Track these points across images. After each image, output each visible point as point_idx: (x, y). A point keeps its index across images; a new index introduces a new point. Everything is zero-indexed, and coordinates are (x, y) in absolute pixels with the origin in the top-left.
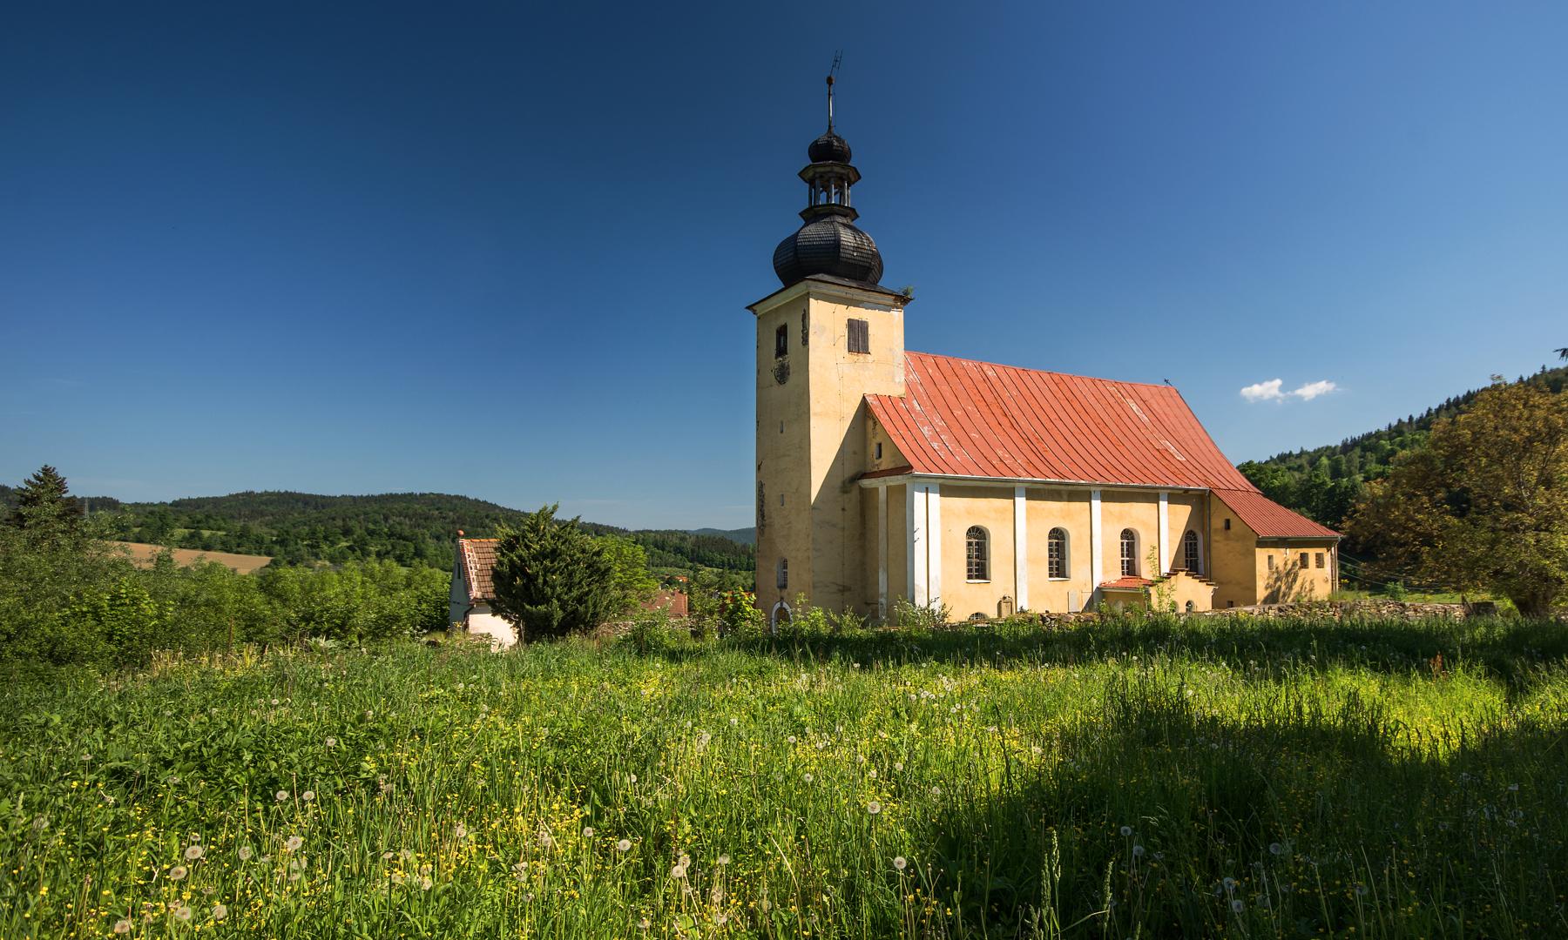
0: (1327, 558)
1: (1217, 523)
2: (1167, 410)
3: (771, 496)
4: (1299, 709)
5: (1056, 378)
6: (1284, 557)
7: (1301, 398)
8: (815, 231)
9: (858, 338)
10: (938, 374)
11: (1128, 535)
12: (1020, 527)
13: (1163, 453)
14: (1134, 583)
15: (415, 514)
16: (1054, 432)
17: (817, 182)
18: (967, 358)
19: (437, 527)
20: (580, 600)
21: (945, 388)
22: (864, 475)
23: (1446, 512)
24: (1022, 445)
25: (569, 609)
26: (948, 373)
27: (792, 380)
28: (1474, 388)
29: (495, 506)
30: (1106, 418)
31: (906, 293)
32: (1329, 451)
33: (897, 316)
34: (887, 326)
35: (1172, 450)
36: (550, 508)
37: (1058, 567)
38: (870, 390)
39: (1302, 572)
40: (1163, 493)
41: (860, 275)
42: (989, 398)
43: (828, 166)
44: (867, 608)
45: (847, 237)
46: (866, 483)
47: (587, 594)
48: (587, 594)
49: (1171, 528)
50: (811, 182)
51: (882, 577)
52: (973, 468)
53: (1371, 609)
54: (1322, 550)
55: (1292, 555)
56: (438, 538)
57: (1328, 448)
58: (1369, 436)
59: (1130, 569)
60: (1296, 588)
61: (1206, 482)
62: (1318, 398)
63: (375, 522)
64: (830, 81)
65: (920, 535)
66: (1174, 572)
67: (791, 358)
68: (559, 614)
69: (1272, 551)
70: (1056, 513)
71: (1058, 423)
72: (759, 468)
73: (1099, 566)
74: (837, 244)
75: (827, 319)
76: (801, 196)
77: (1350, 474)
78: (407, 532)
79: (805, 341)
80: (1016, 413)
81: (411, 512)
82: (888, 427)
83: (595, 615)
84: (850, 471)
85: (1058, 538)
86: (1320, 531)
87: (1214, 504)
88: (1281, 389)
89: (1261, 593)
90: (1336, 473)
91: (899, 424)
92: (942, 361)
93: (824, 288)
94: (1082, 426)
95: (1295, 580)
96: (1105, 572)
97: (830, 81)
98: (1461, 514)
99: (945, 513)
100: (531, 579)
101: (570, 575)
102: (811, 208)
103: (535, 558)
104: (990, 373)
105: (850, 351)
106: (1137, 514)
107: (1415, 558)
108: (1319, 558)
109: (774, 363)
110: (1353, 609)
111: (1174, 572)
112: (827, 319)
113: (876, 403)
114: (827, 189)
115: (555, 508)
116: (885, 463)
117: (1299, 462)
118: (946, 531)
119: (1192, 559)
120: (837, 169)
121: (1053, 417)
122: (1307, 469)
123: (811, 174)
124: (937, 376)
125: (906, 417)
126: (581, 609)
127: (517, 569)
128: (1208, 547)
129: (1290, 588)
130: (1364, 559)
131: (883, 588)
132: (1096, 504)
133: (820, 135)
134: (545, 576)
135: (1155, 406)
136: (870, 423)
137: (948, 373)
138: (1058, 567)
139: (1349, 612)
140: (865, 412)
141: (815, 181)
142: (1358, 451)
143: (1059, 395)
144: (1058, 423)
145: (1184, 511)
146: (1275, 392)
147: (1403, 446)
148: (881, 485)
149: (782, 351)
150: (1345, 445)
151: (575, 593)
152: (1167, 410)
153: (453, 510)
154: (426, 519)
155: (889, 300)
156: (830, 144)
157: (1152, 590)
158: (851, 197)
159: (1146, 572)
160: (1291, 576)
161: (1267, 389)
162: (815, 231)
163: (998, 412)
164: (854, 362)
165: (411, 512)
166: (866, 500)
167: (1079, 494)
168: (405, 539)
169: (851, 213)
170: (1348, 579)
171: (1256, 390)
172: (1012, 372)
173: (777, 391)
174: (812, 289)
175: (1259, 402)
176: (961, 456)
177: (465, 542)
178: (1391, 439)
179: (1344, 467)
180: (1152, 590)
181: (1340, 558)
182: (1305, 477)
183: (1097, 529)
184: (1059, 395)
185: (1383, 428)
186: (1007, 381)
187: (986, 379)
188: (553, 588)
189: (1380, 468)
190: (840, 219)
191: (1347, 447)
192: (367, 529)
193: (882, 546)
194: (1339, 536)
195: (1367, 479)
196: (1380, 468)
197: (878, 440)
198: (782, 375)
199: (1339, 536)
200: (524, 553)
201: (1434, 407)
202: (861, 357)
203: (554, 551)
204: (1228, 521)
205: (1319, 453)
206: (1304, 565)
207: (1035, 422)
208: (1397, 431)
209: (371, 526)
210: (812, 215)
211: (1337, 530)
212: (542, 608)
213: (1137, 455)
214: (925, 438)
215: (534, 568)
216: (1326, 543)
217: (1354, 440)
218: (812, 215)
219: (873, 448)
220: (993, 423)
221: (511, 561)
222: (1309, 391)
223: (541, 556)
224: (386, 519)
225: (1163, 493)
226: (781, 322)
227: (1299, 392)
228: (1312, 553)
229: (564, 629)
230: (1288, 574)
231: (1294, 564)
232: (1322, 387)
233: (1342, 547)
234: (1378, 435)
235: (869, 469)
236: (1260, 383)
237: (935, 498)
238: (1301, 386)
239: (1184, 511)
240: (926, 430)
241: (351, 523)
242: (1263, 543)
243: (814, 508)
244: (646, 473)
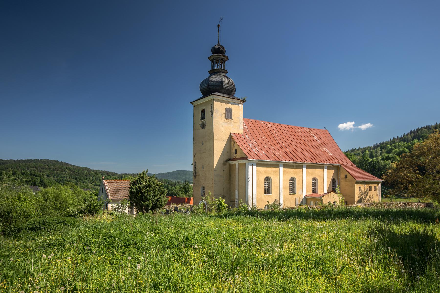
0: (378, 187)
1: (342, 176)
2: (325, 138)
3: (199, 165)
4: (401, 232)
5: (290, 127)
6: (364, 187)
7: (360, 129)
8: (214, 78)
9: (229, 114)
10: (253, 126)
11: (314, 179)
12: (281, 177)
13: (324, 152)
14: (315, 195)
15: (39, 167)
16: (290, 145)
17: (215, 61)
18: (262, 120)
19: (48, 172)
20: (157, 200)
21: (255, 131)
22: (230, 160)
23: (418, 173)
24: (281, 150)
25: (154, 203)
26: (256, 125)
27: (207, 128)
28: (420, 127)
29: (69, 164)
30: (306, 141)
31: (244, 99)
32: (369, 149)
33: (241, 107)
34: (238, 110)
35: (328, 151)
36: (146, 172)
37: (292, 190)
38: (232, 131)
39: (370, 192)
40: (326, 166)
41: (229, 92)
42: (269, 134)
43: (218, 56)
44: (231, 203)
45: (225, 80)
46: (231, 162)
47: (159, 198)
48: (159, 198)
49: (327, 177)
50: (212, 61)
51: (237, 193)
52: (266, 157)
53: (396, 204)
54: (376, 185)
55: (367, 186)
56: (48, 176)
57: (368, 147)
58: (383, 143)
59: (315, 191)
60: (368, 197)
61: (339, 162)
62: (368, 129)
63: (24, 170)
64: (219, 26)
65: (250, 179)
66: (329, 192)
67: (206, 120)
68: (151, 205)
69: (360, 185)
70: (292, 173)
71: (291, 142)
72: (194, 156)
73: (303, 190)
74: (222, 83)
75: (219, 107)
76: (209, 66)
77: (376, 156)
78: (37, 174)
79: (212, 115)
80: (278, 139)
81: (37, 166)
82: (239, 144)
83: (161, 205)
84: (226, 158)
85: (292, 180)
86: (376, 179)
87: (342, 169)
88: (353, 125)
89: (357, 199)
90: (371, 156)
91: (242, 143)
92: (254, 121)
93: (218, 98)
94: (299, 143)
95: (367, 195)
96: (307, 192)
97: (219, 26)
98: (423, 174)
99: (258, 172)
100: (143, 194)
101: (154, 192)
102: (213, 70)
103: (143, 187)
104: (269, 125)
105: (226, 118)
106: (317, 173)
107: (406, 188)
108: (375, 188)
109: (200, 122)
110: (390, 205)
111: (329, 192)
112: (219, 107)
113: (234, 136)
114: (217, 63)
115: (147, 171)
116: (238, 156)
117: (358, 152)
118: (258, 178)
119: (333, 187)
120: (221, 57)
121: (290, 140)
122: (361, 155)
123: (212, 58)
124: (253, 126)
125: (244, 140)
126: (158, 203)
127: (139, 191)
128: (339, 184)
129: (366, 197)
130: (390, 187)
131: (237, 196)
132: (305, 170)
133: (215, 44)
134: (147, 193)
135: (321, 137)
136: (233, 142)
137: (256, 125)
138: (292, 190)
139: (389, 206)
140: (231, 139)
141: (214, 61)
142: (379, 148)
143: (291, 133)
144: (291, 142)
145: (332, 172)
146: (352, 127)
147: (395, 147)
148: (237, 163)
149: (203, 118)
150: (374, 146)
151: (156, 198)
152: (325, 138)
153: (54, 165)
154: (43, 169)
155: (239, 101)
156: (219, 48)
157: (323, 198)
158: (226, 66)
159: (320, 192)
160: (366, 193)
161: (348, 125)
162: (214, 78)
163: (272, 139)
164: (228, 122)
165: (37, 166)
166: (231, 168)
167: (299, 166)
168: (36, 176)
169: (226, 72)
170: (383, 195)
171: (342, 126)
172: (276, 125)
173: (201, 131)
174: (215, 98)
175: (345, 131)
176: (262, 154)
177: (105, 181)
178: (391, 144)
179: (374, 154)
180: (323, 198)
181: (381, 188)
182: (361, 158)
183: (305, 177)
184: (291, 133)
185: (388, 140)
186: (274, 128)
187: (268, 127)
188: (150, 196)
189: (387, 155)
190: (222, 74)
191: (375, 147)
192: (21, 173)
193: (237, 183)
194: (382, 181)
195: (383, 159)
196: (387, 155)
197: (235, 148)
198: (203, 126)
199: (382, 181)
200: (140, 185)
201: (406, 133)
202: (230, 120)
203: (149, 185)
204: (346, 175)
205: (365, 149)
206: (370, 190)
207: (284, 142)
208: (393, 142)
209: (23, 171)
210: (213, 72)
211: (381, 179)
212: (147, 203)
213: (317, 153)
214: (248, 147)
215: (143, 190)
216: (377, 183)
217: (377, 144)
218: (213, 72)
219: (234, 151)
220: (271, 143)
221: (136, 188)
222: (364, 127)
223: (146, 187)
224: (28, 169)
225: (326, 166)
226: (203, 108)
227: (360, 127)
228: (373, 186)
229: (153, 208)
230: (365, 193)
231: (367, 189)
232: (368, 125)
233: (383, 184)
234: (386, 143)
235: (232, 157)
236: (346, 123)
237: (255, 168)
238: (361, 125)
239: (332, 172)
240: (250, 145)
241: (15, 170)
242: (357, 183)
243: (215, 170)
244: (171, 159)
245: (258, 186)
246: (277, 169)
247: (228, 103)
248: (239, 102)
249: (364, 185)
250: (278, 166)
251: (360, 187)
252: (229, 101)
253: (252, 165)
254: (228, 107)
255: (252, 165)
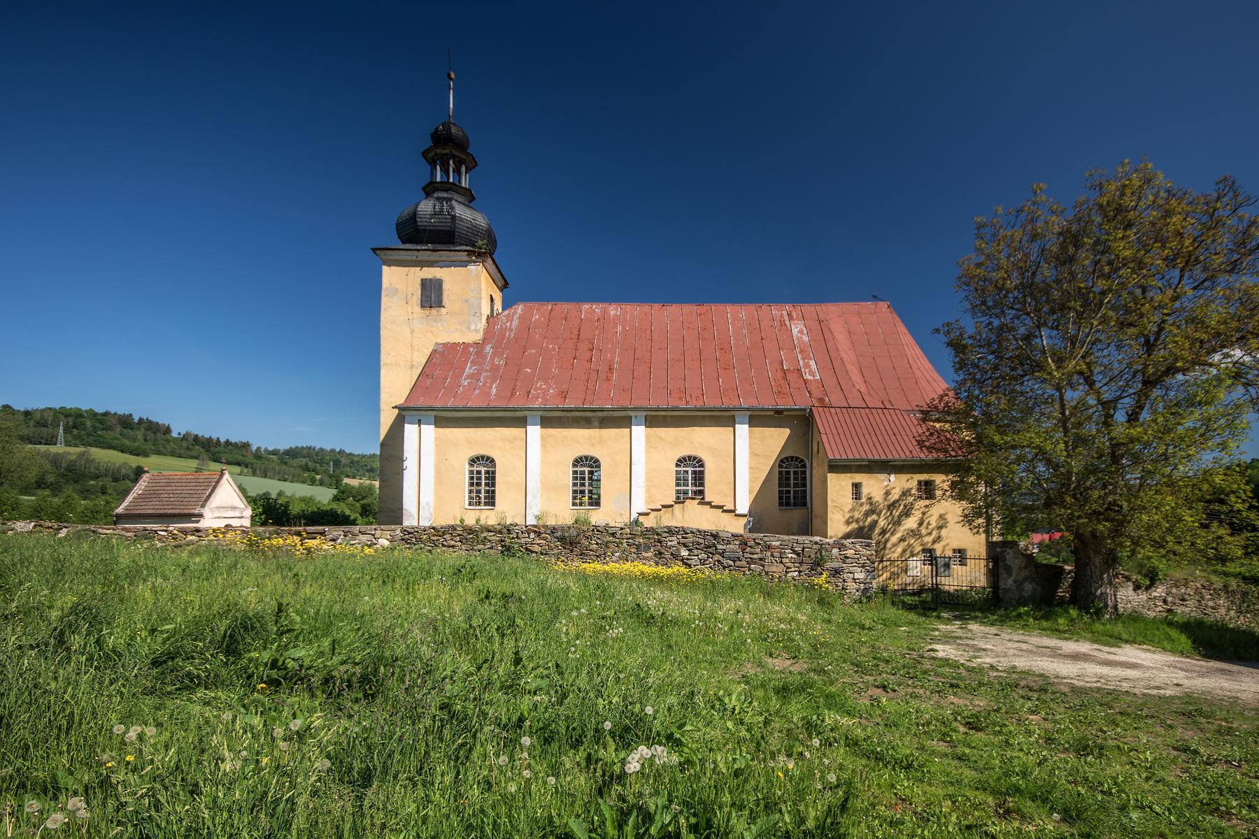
9: (431, 295)
49: (753, 454)
70: (582, 441)
106: (700, 440)
132: (743, 429)
145: (776, 439)
202: (434, 311)
237: (429, 430)
245: (439, 480)
246: (516, 432)
247: (431, 264)
248: (466, 258)
249: (882, 476)
250: (521, 422)
251: (857, 487)
252: (432, 258)
253: (419, 423)
254: (430, 276)
255: (419, 423)
